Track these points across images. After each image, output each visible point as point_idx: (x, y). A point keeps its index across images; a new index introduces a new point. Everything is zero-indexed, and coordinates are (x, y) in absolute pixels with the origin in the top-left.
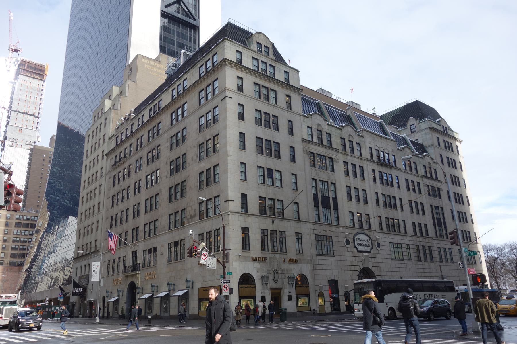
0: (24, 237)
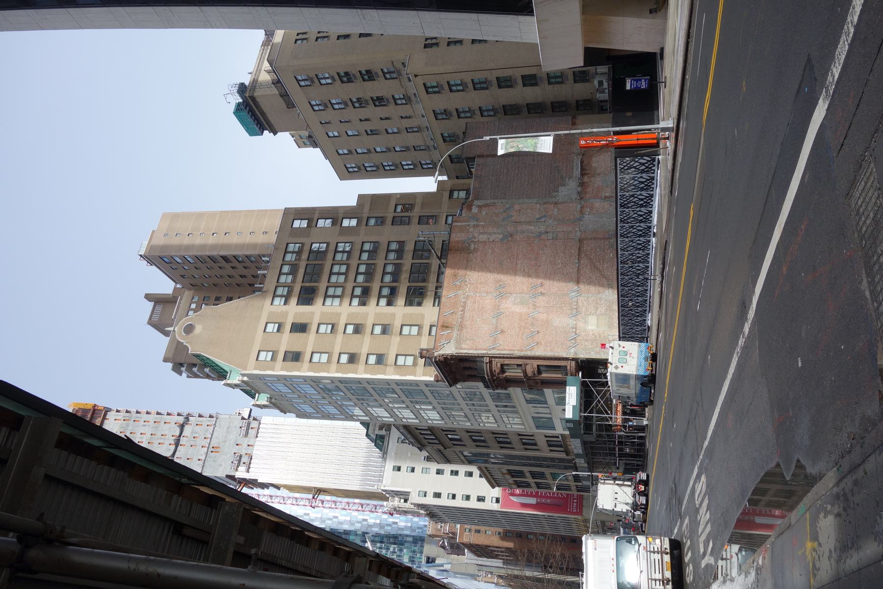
0: (352, 275)
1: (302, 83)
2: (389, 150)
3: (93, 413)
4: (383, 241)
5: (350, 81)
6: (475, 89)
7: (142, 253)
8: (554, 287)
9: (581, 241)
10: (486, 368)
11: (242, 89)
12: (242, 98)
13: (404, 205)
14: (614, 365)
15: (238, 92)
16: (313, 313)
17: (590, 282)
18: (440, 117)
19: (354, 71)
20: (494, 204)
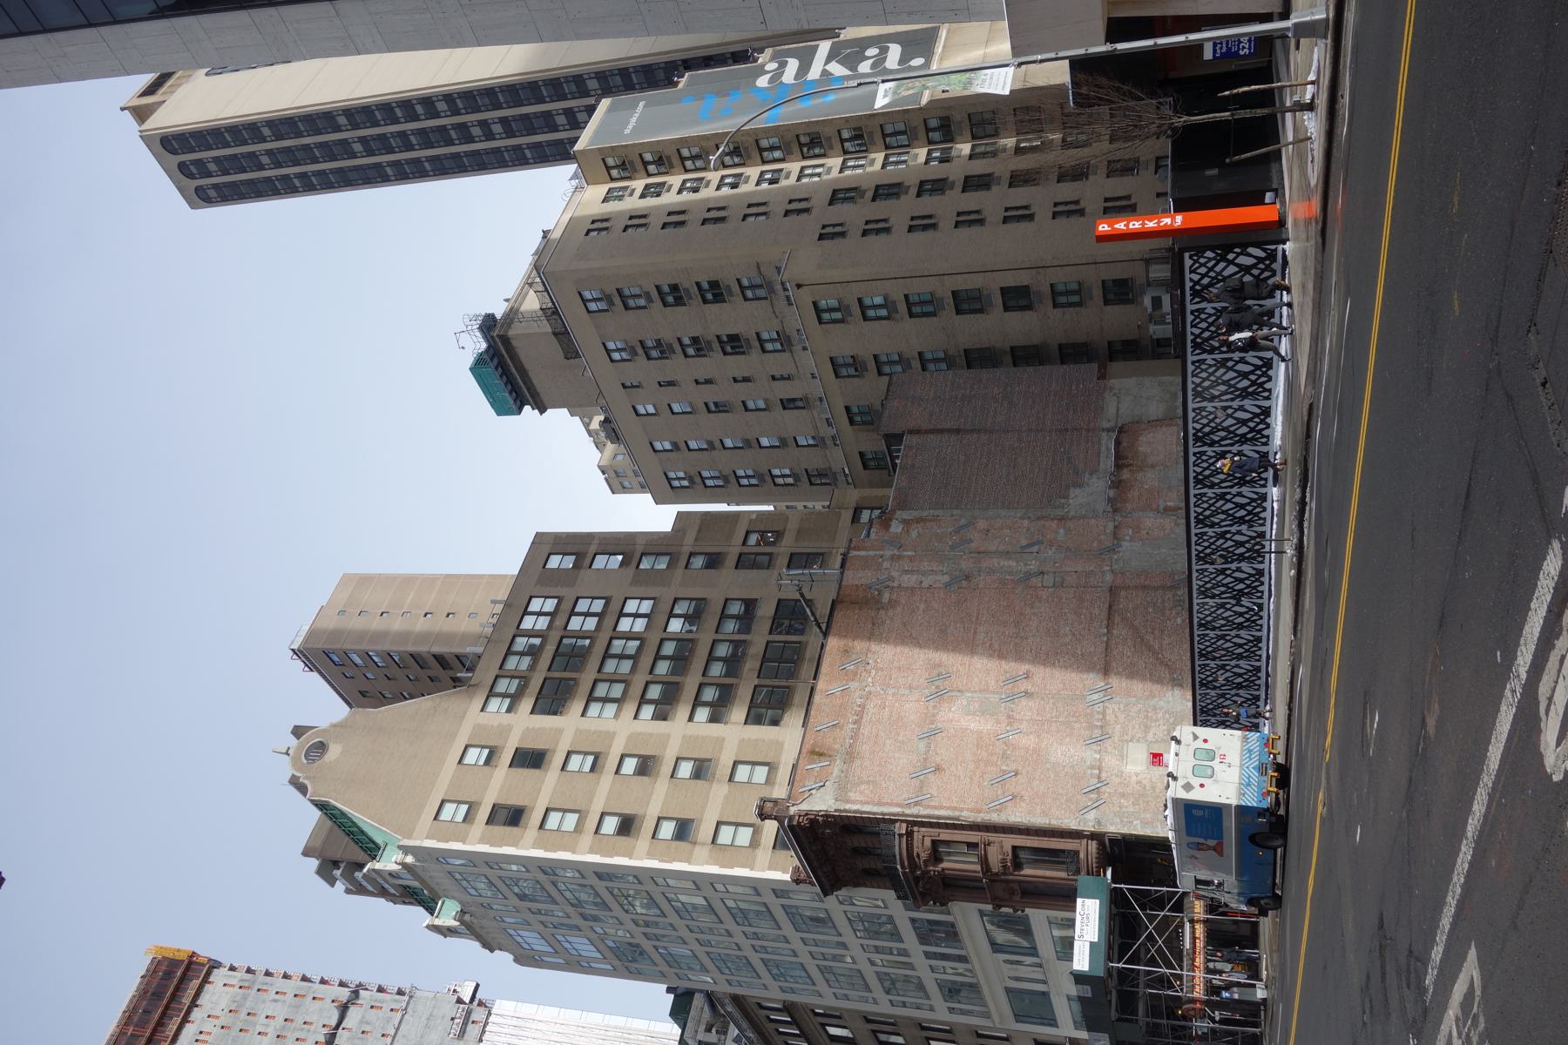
0: (646, 661)
1: (593, 306)
2: (748, 444)
3: (188, 969)
4: (716, 598)
5: (679, 301)
6: (911, 315)
7: (295, 647)
8: (1053, 680)
9: (1113, 591)
10: (899, 847)
11: (488, 325)
12: (487, 341)
13: (763, 533)
14: (1181, 782)
15: (481, 328)
16: (560, 731)
17: (1132, 673)
18: (844, 372)
19: (687, 283)
20: (936, 519)
